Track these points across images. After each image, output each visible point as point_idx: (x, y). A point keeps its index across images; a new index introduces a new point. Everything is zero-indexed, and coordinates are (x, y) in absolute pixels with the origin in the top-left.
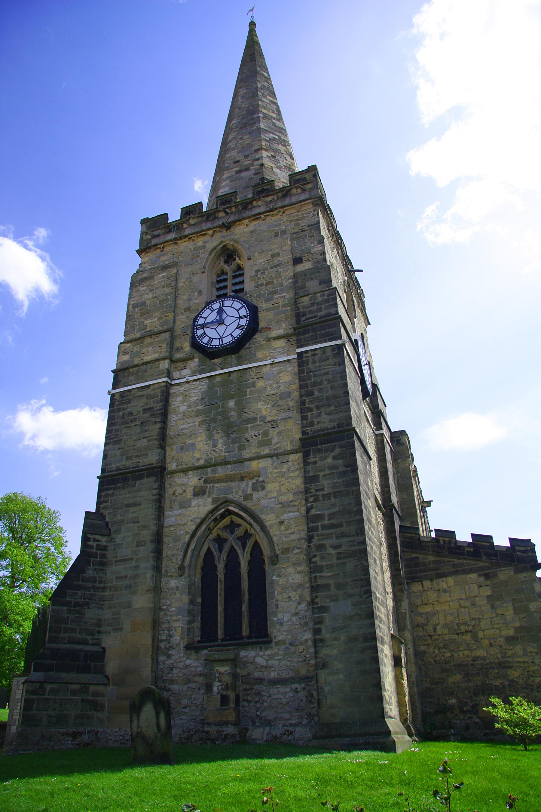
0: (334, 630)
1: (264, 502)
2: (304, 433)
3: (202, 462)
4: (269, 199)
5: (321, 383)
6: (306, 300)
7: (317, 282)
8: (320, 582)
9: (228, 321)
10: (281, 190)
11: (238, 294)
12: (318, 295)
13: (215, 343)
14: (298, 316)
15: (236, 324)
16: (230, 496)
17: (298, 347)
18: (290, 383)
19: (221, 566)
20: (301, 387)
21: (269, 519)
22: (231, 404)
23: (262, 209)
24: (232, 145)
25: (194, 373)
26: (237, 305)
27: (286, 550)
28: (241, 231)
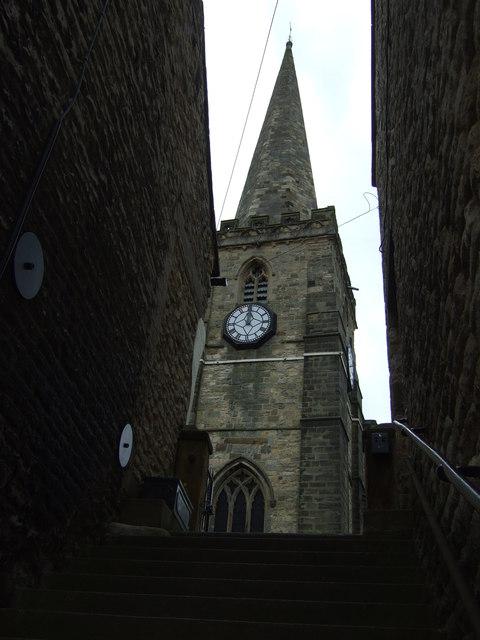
1: (269, 462)
2: (303, 416)
3: (224, 427)
4: (294, 228)
5: (320, 381)
6: (315, 317)
7: (324, 303)
8: (304, 523)
9: (253, 323)
10: (304, 222)
11: (261, 301)
12: (325, 315)
13: (242, 338)
14: (308, 328)
15: (259, 326)
16: (243, 455)
17: (306, 352)
19: (231, 504)
20: (305, 382)
21: (272, 475)
22: (251, 386)
23: (288, 236)
25: (223, 358)
26: (262, 311)
27: (283, 498)
28: (268, 252)
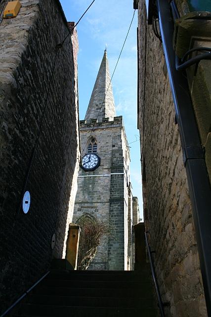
0: (114, 251)
3: (81, 202)
5: (117, 184)
9: (92, 161)
10: (111, 122)
13: (87, 167)
18: (108, 183)
20: (111, 185)
22: (91, 186)
23: (105, 127)
24: (96, 98)
28: (98, 133)
